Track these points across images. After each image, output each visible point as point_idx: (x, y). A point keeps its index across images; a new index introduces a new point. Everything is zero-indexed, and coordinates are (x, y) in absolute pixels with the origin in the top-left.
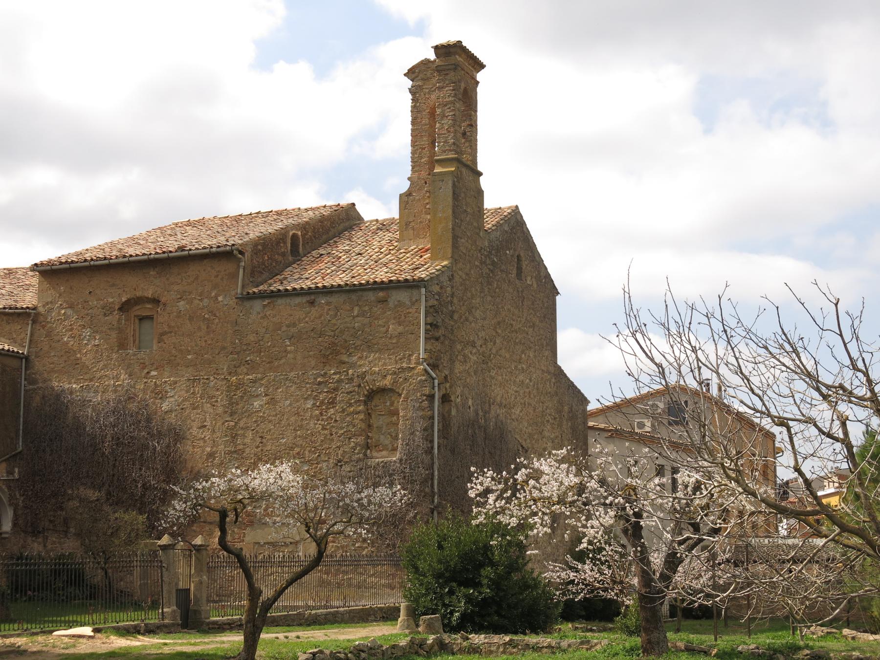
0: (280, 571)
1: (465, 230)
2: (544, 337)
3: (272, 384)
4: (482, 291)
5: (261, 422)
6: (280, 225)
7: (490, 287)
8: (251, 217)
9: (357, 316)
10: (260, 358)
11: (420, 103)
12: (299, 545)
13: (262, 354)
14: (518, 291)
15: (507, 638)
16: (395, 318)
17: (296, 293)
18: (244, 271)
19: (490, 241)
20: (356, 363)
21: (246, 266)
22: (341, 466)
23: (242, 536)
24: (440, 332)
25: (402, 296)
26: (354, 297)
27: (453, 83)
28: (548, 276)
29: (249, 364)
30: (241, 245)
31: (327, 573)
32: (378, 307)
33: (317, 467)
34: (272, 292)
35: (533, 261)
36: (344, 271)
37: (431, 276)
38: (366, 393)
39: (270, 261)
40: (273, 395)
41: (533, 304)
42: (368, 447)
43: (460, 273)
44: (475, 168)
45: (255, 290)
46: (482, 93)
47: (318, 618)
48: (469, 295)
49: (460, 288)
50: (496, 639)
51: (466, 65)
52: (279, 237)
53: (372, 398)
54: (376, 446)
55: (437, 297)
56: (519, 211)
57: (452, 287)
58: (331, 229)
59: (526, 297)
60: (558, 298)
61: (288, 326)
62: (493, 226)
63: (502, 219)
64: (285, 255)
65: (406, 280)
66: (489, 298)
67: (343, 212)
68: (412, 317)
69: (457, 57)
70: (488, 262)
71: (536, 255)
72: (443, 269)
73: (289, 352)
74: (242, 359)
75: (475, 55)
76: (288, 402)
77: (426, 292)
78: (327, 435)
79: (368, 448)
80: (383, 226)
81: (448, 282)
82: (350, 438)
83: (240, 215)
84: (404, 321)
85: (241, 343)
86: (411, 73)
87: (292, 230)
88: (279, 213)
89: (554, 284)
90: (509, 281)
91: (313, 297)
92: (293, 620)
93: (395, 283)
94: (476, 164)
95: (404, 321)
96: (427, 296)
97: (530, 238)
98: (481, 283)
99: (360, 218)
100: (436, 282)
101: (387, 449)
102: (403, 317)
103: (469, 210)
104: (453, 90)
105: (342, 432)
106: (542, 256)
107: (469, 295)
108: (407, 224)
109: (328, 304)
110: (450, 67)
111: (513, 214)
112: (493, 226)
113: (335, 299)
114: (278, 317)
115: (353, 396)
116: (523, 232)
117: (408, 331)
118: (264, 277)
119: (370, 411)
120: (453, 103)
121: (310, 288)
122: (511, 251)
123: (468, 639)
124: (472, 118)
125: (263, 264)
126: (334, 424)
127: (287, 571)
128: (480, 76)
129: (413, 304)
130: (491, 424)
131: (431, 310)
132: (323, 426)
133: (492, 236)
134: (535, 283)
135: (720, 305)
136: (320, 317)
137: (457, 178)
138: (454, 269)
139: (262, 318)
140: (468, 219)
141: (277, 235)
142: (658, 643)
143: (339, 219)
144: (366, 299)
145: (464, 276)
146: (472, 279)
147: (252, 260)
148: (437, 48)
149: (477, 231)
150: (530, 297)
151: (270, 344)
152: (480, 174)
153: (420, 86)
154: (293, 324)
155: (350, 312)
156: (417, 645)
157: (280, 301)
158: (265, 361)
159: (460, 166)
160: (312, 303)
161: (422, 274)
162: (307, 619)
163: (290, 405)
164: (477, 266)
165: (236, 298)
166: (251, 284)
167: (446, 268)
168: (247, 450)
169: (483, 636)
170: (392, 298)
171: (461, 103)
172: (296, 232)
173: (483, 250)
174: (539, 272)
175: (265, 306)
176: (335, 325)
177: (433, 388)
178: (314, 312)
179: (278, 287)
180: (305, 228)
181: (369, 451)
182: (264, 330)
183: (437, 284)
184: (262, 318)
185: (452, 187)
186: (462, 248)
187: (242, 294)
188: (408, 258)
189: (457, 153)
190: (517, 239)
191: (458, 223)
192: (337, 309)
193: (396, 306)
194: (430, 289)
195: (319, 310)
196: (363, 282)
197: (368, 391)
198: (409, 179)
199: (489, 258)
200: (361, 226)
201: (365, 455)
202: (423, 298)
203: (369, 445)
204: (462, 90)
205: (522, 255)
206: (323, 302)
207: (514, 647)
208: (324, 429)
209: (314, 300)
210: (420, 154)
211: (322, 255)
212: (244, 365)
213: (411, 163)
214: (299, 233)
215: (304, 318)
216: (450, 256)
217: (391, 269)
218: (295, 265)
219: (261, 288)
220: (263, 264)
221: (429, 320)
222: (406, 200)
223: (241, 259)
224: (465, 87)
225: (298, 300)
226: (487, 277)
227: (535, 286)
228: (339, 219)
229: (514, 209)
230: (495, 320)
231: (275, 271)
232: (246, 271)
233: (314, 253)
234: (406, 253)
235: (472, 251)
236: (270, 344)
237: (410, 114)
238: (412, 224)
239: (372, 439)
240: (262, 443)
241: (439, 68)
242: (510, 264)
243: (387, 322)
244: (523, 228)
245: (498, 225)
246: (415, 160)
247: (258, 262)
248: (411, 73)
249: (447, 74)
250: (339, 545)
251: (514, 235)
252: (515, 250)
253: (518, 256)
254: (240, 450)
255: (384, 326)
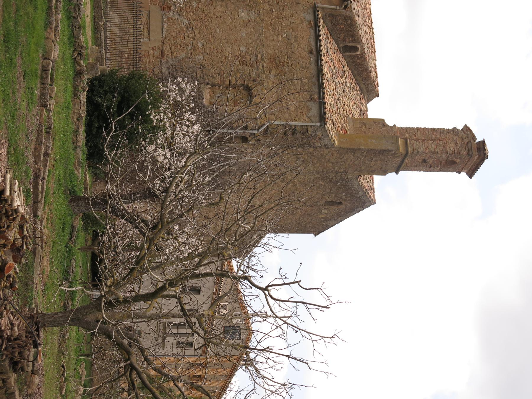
0: (130, 26)
1: (359, 159)
2: (286, 223)
3: (257, 25)
4: (318, 172)
5: (231, 17)
6: (364, 40)
7: (320, 179)
8: (369, 17)
9: (301, 81)
10: (274, 18)
11: (446, 134)
12: (147, 39)
13: (277, 19)
14: (317, 202)
15: (83, 115)
16: (299, 105)
17: (318, 42)
18: (333, 9)
19: (351, 180)
20: (269, 80)
21: (336, 11)
22: (200, 68)
23: (155, 3)
24: (290, 138)
25: (314, 110)
26: (315, 79)
27: (459, 152)
28: (327, 227)
29: (270, 10)
30: (351, 6)
31: (128, 57)
32: (308, 95)
33: (200, 52)
34: (319, 27)
35: (338, 215)
36: (332, 77)
37: (328, 131)
38: (250, 85)
39: (340, 29)
40: (249, 26)
41: (308, 214)
42: (213, 86)
43: (330, 154)
44: (401, 169)
45: (320, 16)
46: (454, 175)
47: (99, 32)
48: (315, 161)
49: (319, 154)
50: (83, 108)
51: (470, 164)
52: (356, 37)
53: (246, 90)
54: (213, 91)
55: (314, 134)
56: (372, 205)
57: (320, 147)
58: (361, 78)
59: (313, 208)
60: (312, 235)
61: (295, 37)
62: (362, 183)
63: (366, 190)
64: (344, 41)
65: (325, 113)
66: (312, 178)
67: (373, 88)
68: (300, 117)
69: (477, 156)
70: (338, 178)
71: (341, 217)
72: (332, 140)
73: (278, 37)
74: (273, 6)
75: (479, 170)
76: (244, 35)
77: (317, 126)
78: (221, 59)
79: (212, 86)
80: (363, 112)
81: (323, 144)
82: (219, 74)
83: (372, 21)
84: (297, 112)
85: (284, 6)
86: (466, 129)
87: (361, 47)
88: (373, 46)
89: (321, 232)
90: (324, 195)
91: (315, 53)
92: (98, 12)
93: (323, 96)
94: (404, 170)
95: (297, 112)
96: (314, 127)
97: (353, 213)
98: (323, 172)
99: (369, 100)
100: (324, 134)
101: (211, 99)
102: (300, 111)
103: (372, 162)
104: (455, 153)
105: (223, 69)
106: (341, 223)
107: (315, 161)
108: (364, 124)
109: (310, 63)
110: (470, 151)
111: (370, 199)
112: (362, 183)
113: (313, 67)
114: (301, 30)
115: (248, 77)
116: (357, 207)
117: (291, 114)
118: (329, 24)
119: (237, 88)
120: (446, 152)
121: (321, 51)
122: (344, 197)
123: (84, 91)
124: (436, 168)
125: (338, 24)
126: (228, 64)
127: (130, 26)
128: (464, 175)
129: (309, 118)
130: (227, 177)
131: (305, 130)
132: (228, 57)
133: (355, 182)
134: (323, 216)
135: (308, 289)
136: (301, 57)
137: (393, 153)
138: (333, 149)
139: (301, 20)
140: (367, 162)
141: (357, 35)
142: (78, 206)
143: (368, 84)
144: (313, 87)
145: (327, 157)
146: (326, 164)
147: (340, 15)
148: (483, 142)
149: (358, 169)
150: (313, 212)
151: (284, 24)
152: (397, 173)
153: (458, 134)
154: (297, 40)
155: (304, 77)
156: (80, 51)
157: (312, 32)
158: (272, 21)
159: (403, 156)
160: (311, 52)
161: (329, 125)
162: (98, 23)
163: (242, 36)
164: (335, 168)
165: (315, 3)
166: (324, 14)
167: (333, 143)
168: (212, 8)
169: (85, 100)
170: (314, 105)
171: (446, 159)
172: (359, 50)
173: (345, 174)
174: (330, 220)
175: (309, 22)
176: (296, 67)
177: (251, 130)
178: (305, 54)
179: (321, 31)
180: (362, 57)
181: (210, 86)
182: (293, 21)
183: (322, 135)
184: (301, 20)
185: (388, 149)
186: (347, 156)
187: (318, 7)
188: (341, 121)
189: (412, 154)
190: (352, 202)
191: (364, 153)
192: (306, 68)
193: (308, 107)
194: (319, 129)
195: (306, 57)
196: (324, 86)
197: (251, 86)
198: (395, 125)
199: (340, 179)
200: (363, 99)
201: (208, 83)
202: (313, 124)
203: (214, 87)
204: (454, 159)
205: (342, 206)
206: (311, 60)
207: (77, 119)
208: (226, 57)
209: (313, 54)
210: (411, 133)
211: (344, 67)
212: (270, 7)
213: (405, 127)
214: (359, 53)
215: (300, 47)
216: (342, 146)
217: (333, 107)
218: (336, 48)
219: (322, 21)
220: (338, 24)
221: (298, 128)
222: (381, 123)
223: (342, 7)
224: (456, 163)
225: (313, 43)
226: (327, 176)
227: (321, 216)
228: (368, 84)
229: (373, 201)
230: (297, 183)
231: (333, 32)
232: (333, 10)
233: (345, 63)
234: (344, 121)
235: (344, 164)
236: (284, 24)
237: (439, 127)
238: (364, 127)
239: (218, 89)
240: (217, 17)
241: (469, 144)
242: (336, 196)
243: (297, 100)
244: (361, 207)
245: (362, 187)
246: (407, 130)
247: (339, 20)
248: (466, 129)
249: (465, 149)
250: (147, 65)
251: (355, 200)
252: (345, 200)
253: (341, 202)
254: (212, 3)
255: (294, 99)
